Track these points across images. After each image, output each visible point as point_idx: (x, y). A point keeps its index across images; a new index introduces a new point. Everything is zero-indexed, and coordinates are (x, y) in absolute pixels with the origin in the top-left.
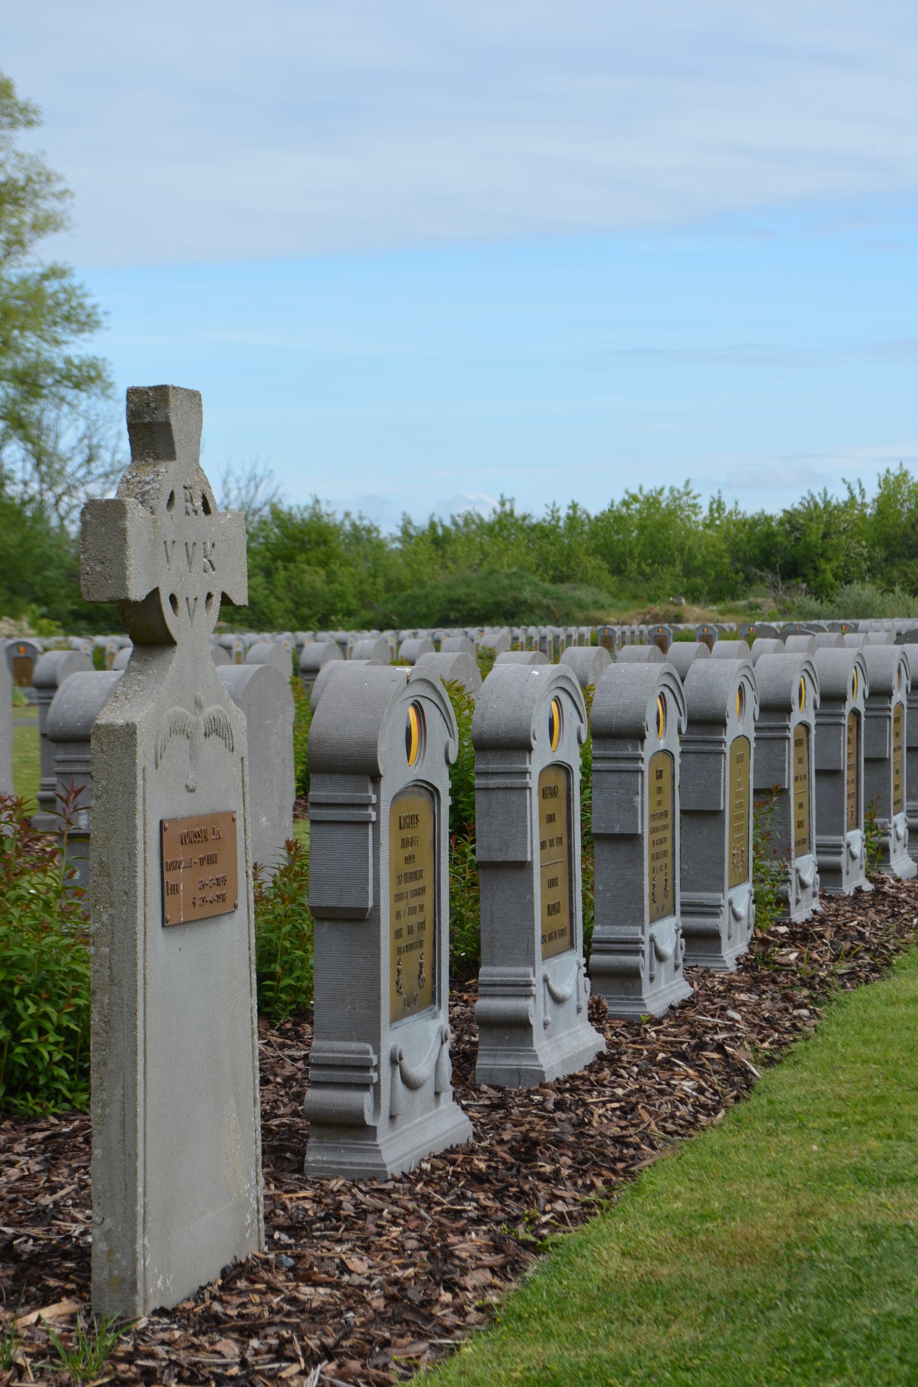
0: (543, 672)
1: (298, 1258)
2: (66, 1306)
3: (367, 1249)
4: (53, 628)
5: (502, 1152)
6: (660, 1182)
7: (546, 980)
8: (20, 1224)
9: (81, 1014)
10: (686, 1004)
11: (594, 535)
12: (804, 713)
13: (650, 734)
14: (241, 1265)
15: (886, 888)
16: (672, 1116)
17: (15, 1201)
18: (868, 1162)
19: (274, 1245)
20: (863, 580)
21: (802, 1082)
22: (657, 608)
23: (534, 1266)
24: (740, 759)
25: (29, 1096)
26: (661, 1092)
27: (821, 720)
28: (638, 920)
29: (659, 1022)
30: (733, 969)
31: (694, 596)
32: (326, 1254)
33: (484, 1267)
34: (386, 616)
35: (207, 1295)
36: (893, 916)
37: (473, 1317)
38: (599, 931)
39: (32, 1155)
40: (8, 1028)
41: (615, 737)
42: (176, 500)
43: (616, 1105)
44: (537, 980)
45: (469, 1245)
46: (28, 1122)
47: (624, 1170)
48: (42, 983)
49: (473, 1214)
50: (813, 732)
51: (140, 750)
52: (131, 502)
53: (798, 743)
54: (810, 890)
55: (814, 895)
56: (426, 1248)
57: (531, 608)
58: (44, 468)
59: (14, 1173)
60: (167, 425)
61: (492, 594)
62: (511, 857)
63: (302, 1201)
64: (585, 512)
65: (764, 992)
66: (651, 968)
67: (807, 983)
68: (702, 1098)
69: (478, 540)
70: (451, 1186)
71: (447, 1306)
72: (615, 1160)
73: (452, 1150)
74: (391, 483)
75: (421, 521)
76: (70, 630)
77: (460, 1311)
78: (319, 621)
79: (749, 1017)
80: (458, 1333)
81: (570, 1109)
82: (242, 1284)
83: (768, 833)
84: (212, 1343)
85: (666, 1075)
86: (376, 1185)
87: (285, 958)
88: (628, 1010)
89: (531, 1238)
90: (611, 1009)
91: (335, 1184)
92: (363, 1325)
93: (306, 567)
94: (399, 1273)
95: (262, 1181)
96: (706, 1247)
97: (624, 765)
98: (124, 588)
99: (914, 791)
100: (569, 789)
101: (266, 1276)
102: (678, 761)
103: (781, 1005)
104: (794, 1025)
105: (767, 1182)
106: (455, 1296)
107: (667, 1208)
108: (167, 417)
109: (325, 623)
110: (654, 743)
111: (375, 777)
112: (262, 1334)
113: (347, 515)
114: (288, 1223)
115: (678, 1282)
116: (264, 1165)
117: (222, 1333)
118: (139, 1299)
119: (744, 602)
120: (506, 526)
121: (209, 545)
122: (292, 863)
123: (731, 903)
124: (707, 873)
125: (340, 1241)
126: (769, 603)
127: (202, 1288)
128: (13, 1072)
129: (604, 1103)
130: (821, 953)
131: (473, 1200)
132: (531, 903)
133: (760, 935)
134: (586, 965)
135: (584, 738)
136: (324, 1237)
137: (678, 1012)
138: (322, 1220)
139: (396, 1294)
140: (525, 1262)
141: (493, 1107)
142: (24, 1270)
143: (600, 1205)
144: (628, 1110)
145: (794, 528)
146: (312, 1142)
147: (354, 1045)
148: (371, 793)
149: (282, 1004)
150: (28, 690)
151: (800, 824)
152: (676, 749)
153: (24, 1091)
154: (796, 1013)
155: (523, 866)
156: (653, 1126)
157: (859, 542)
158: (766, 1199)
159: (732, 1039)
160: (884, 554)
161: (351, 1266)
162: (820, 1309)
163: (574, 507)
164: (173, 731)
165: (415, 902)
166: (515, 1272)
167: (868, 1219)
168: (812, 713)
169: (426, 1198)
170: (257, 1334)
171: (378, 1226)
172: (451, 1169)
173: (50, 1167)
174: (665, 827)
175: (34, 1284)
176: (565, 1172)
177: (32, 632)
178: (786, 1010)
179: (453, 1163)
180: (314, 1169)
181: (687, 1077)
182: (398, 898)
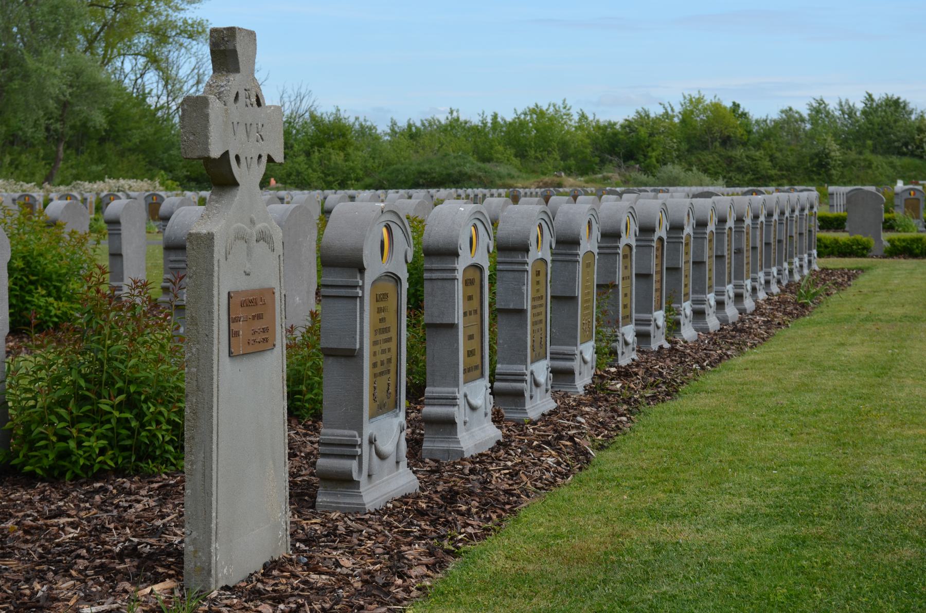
0: (465, 209)
1: (310, 558)
2: (168, 584)
3: (352, 554)
4: (174, 186)
5: (436, 498)
6: (531, 516)
7: (466, 396)
8: (142, 536)
9: (180, 412)
10: (552, 413)
11: (508, 133)
12: (628, 239)
13: (533, 248)
14: (275, 561)
15: (678, 347)
16: (541, 478)
17: (139, 523)
18: (657, 506)
19: (297, 550)
20: (673, 163)
21: (620, 459)
22: (547, 179)
23: (453, 565)
24: (588, 265)
25: (150, 462)
26: (535, 464)
27: (639, 243)
28: (524, 362)
29: (535, 423)
30: (582, 393)
31: (569, 171)
32: (327, 556)
33: (422, 564)
34: (380, 181)
35: (254, 579)
36: (681, 363)
37: (415, 593)
38: (500, 368)
39: (151, 496)
40: (137, 420)
41: (511, 250)
42: (240, 98)
43: (507, 471)
44: (460, 396)
45: (413, 552)
46: (149, 477)
47: (510, 509)
48: (158, 394)
49: (417, 534)
50: (634, 250)
51: (216, 249)
52: (212, 97)
53: (625, 257)
54: (631, 347)
55: (633, 350)
56: (387, 554)
57: (470, 178)
58: (170, 87)
59: (140, 507)
60: (235, 52)
61: (446, 168)
62: (445, 321)
63: (314, 525)
64: (503, 119)
65: (600, 406)
66: (531, 391)
67: (626, 401)
68: (559, 468)
69: (437, 135)
70: (405, 517)
71: (399, 587)
72: (504, 504)
73: (406, 496)
74: (382, 98)
75: (402, 123)
76: (185, 187)
77: (407, 590)
78: (339, 184)
79: (590, 421)
80: (405, 603)
81: (478, 474)
82: (275, 573)
83: (606, 311)
84: (256, 606)
85: (539, 454)
86: (359, 516)
87: (309, 382)
88: (517, 416)
89: (452, 548)
90: (507, 415)
91: (334, 516)
92: (348, 597)
93: (331, 150)
94: (371, 568)
95: (290, 514)
96: (556, 554)
97: (516, 267)
98: (207, 150)
99: (697, 288)
100: (482, 280)
101: (290, 568)
102: (550, 265)
103: (610, 414)
104: (617, 426)
105: (595, 517)
106: (404, 581)
107: (534, 531)
108: (235, 47)
109: (343, 185)
110: (535, 254)
111: (362, 270)
112: (286, 601)
113: (357, 119)
114: (304, 538)
115: (539, 574)
116: (291, 504)
117: (262, 600)
118: (212, 580)
119: (600, 176)
120: (454, 127)
121: (260, 125)
122: (313, 325)
123: (581, 353)
124: (566, 334)
125: (336, 549)
126: (615, 176)
127: (251, 575)
128: (140, 447)
129: (500, 470)
130: (635, 384)
131: (417, 525)
132: (457, 349)
133: (599, 373)
134: (491, 388)
135: (491, 250)
136: (326, 546)
137: (546, 418)
138: (326, 536)
139: (369, 580)
140: (448, 562)
141: (432, 472)
142: (143, 563)
143: (495, 530)
144: (514, 474)
145: (632, 131)
146: (320, 490)
147: (347, 432)
148: (359, 279)
149: (302, 407)
150: (158, 223)
151: (625, 306)
152: (549, 258)
153: (147, 459)
154: (619, 419)
155: (453, 326)
156: (529, 484)
157: (671, 140)
158: (594, 527)
159: (579, 434)
160: (687, 147)
161: (342, 563)
162: (623, 590)
163: (495, 117)
164: (237, 238)
165: (385, 346)
166: (441, 568)
167: (654, 537)
168: (634, 239)
169: (389, 525)
170: (283, 602)
171: (359, 540)
172: (405, 507)
173: (162, 503)
174: (541, 305)
175: (150, 571)
176: (474, 510)
177: (161, 188)
178: (613, 417)
179: (406, 503)
180: (322, 506)
181: (550, 456)
182: (375, 343)
